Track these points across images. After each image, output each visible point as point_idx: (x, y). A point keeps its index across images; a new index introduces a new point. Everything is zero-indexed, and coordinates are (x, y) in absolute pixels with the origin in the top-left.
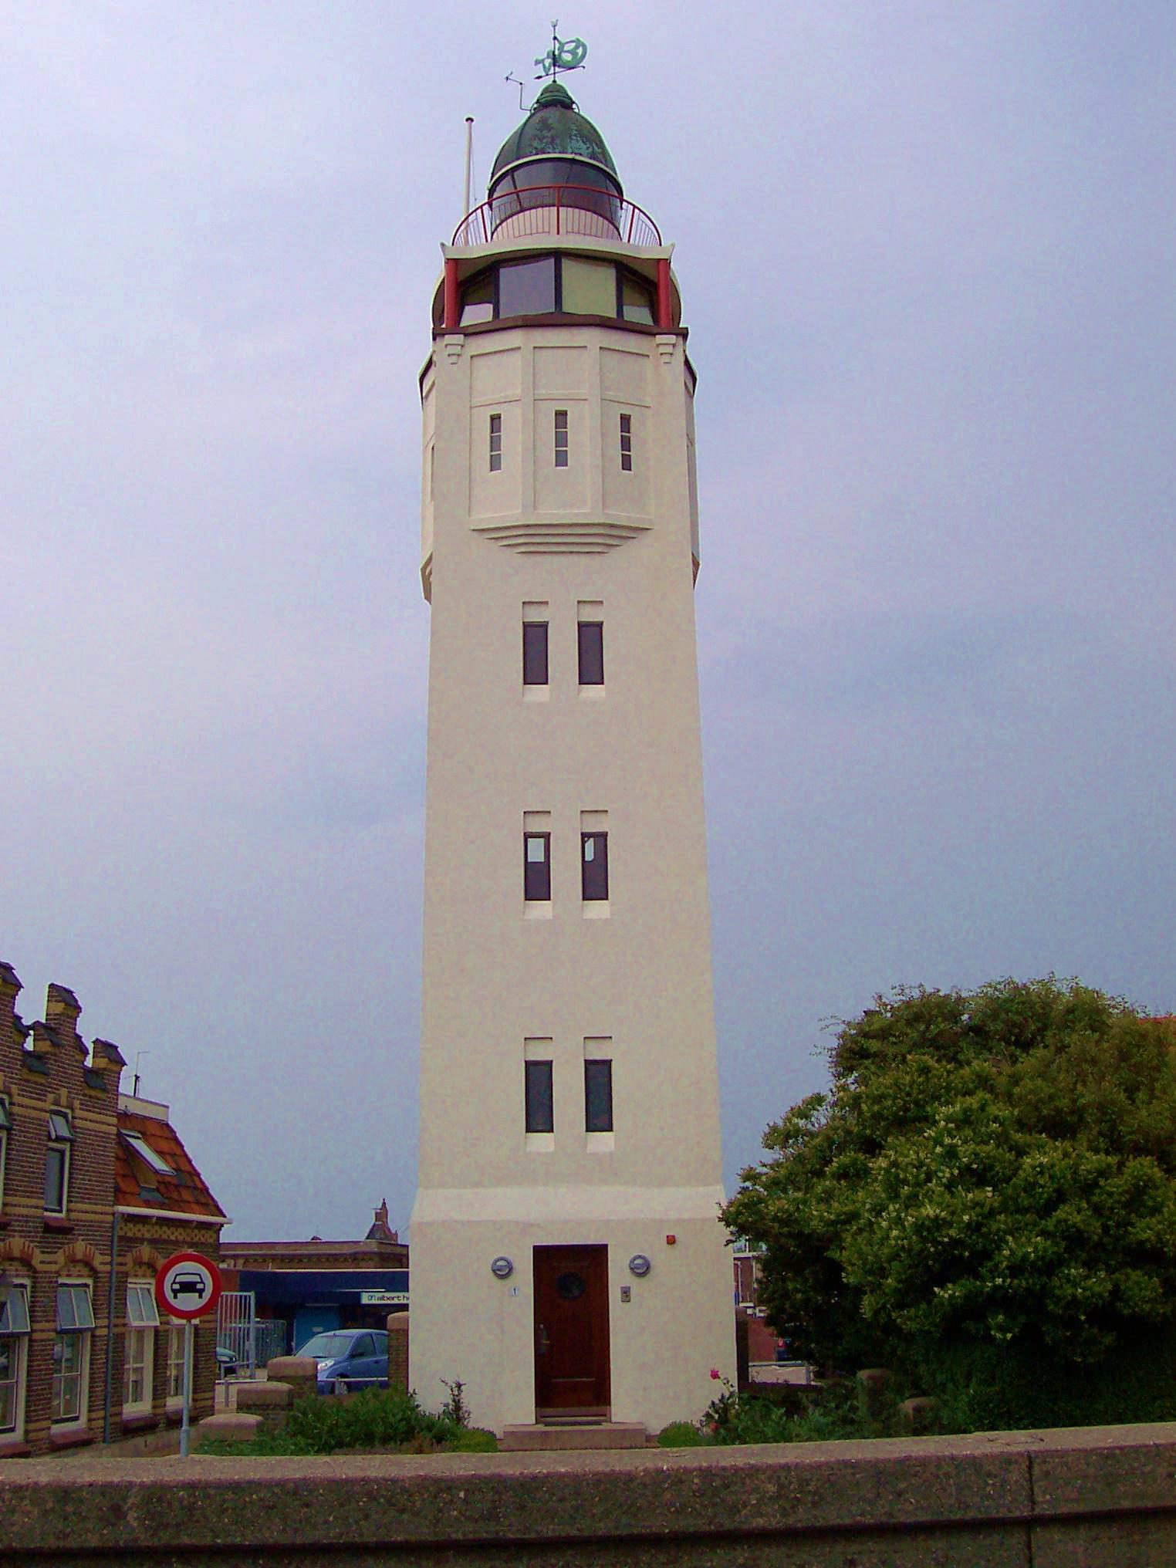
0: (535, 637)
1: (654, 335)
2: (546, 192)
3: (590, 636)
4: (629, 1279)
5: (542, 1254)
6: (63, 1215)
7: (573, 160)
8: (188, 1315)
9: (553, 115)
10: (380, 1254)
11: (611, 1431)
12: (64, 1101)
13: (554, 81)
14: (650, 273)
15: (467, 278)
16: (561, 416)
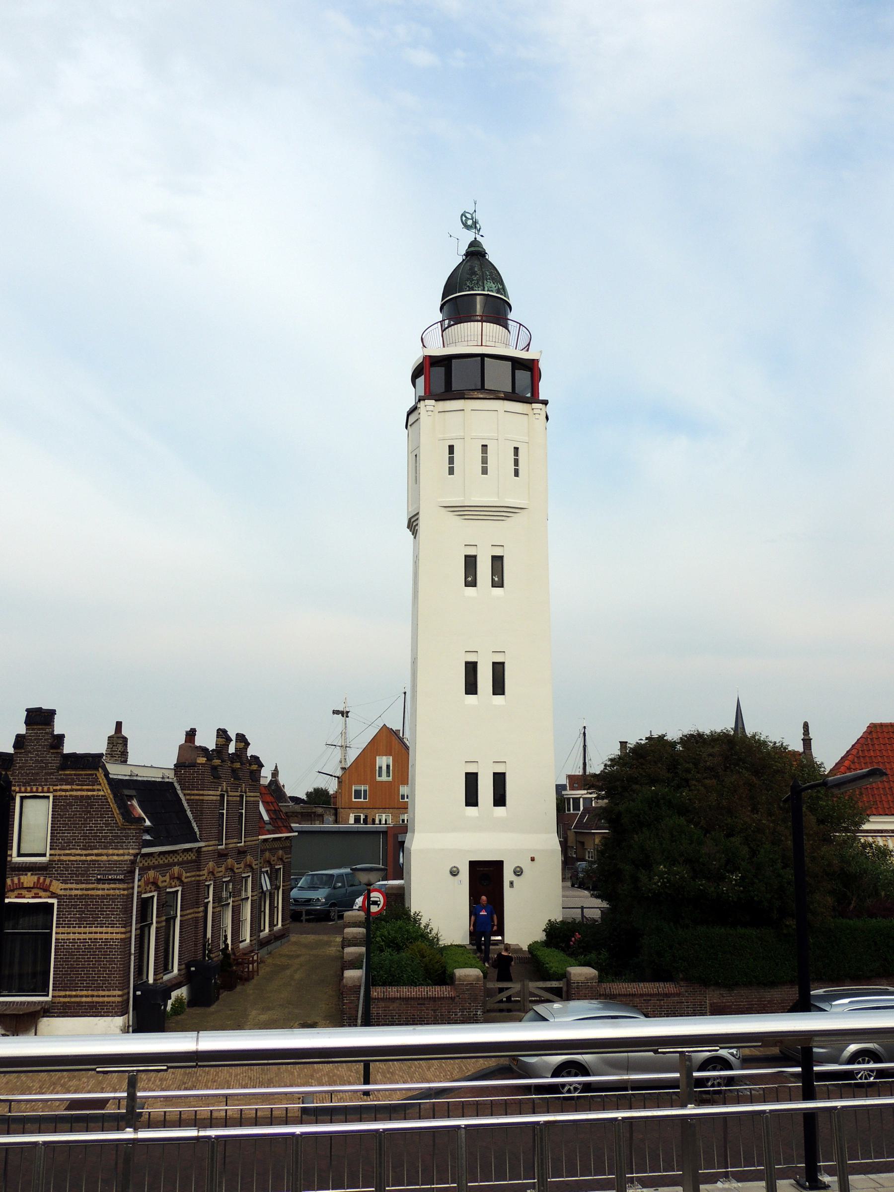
0: (471, 562)
1: (531, 403)
2: (860, 1187)
3: (497, 561)
4: (513, 877)
5: (473, 865)
6: (223, 847)
7: (488, 294)
9: (476, 264)
12: (224, 789)
13: (475, 238)
15: (445, 379)
16: (485, 447)
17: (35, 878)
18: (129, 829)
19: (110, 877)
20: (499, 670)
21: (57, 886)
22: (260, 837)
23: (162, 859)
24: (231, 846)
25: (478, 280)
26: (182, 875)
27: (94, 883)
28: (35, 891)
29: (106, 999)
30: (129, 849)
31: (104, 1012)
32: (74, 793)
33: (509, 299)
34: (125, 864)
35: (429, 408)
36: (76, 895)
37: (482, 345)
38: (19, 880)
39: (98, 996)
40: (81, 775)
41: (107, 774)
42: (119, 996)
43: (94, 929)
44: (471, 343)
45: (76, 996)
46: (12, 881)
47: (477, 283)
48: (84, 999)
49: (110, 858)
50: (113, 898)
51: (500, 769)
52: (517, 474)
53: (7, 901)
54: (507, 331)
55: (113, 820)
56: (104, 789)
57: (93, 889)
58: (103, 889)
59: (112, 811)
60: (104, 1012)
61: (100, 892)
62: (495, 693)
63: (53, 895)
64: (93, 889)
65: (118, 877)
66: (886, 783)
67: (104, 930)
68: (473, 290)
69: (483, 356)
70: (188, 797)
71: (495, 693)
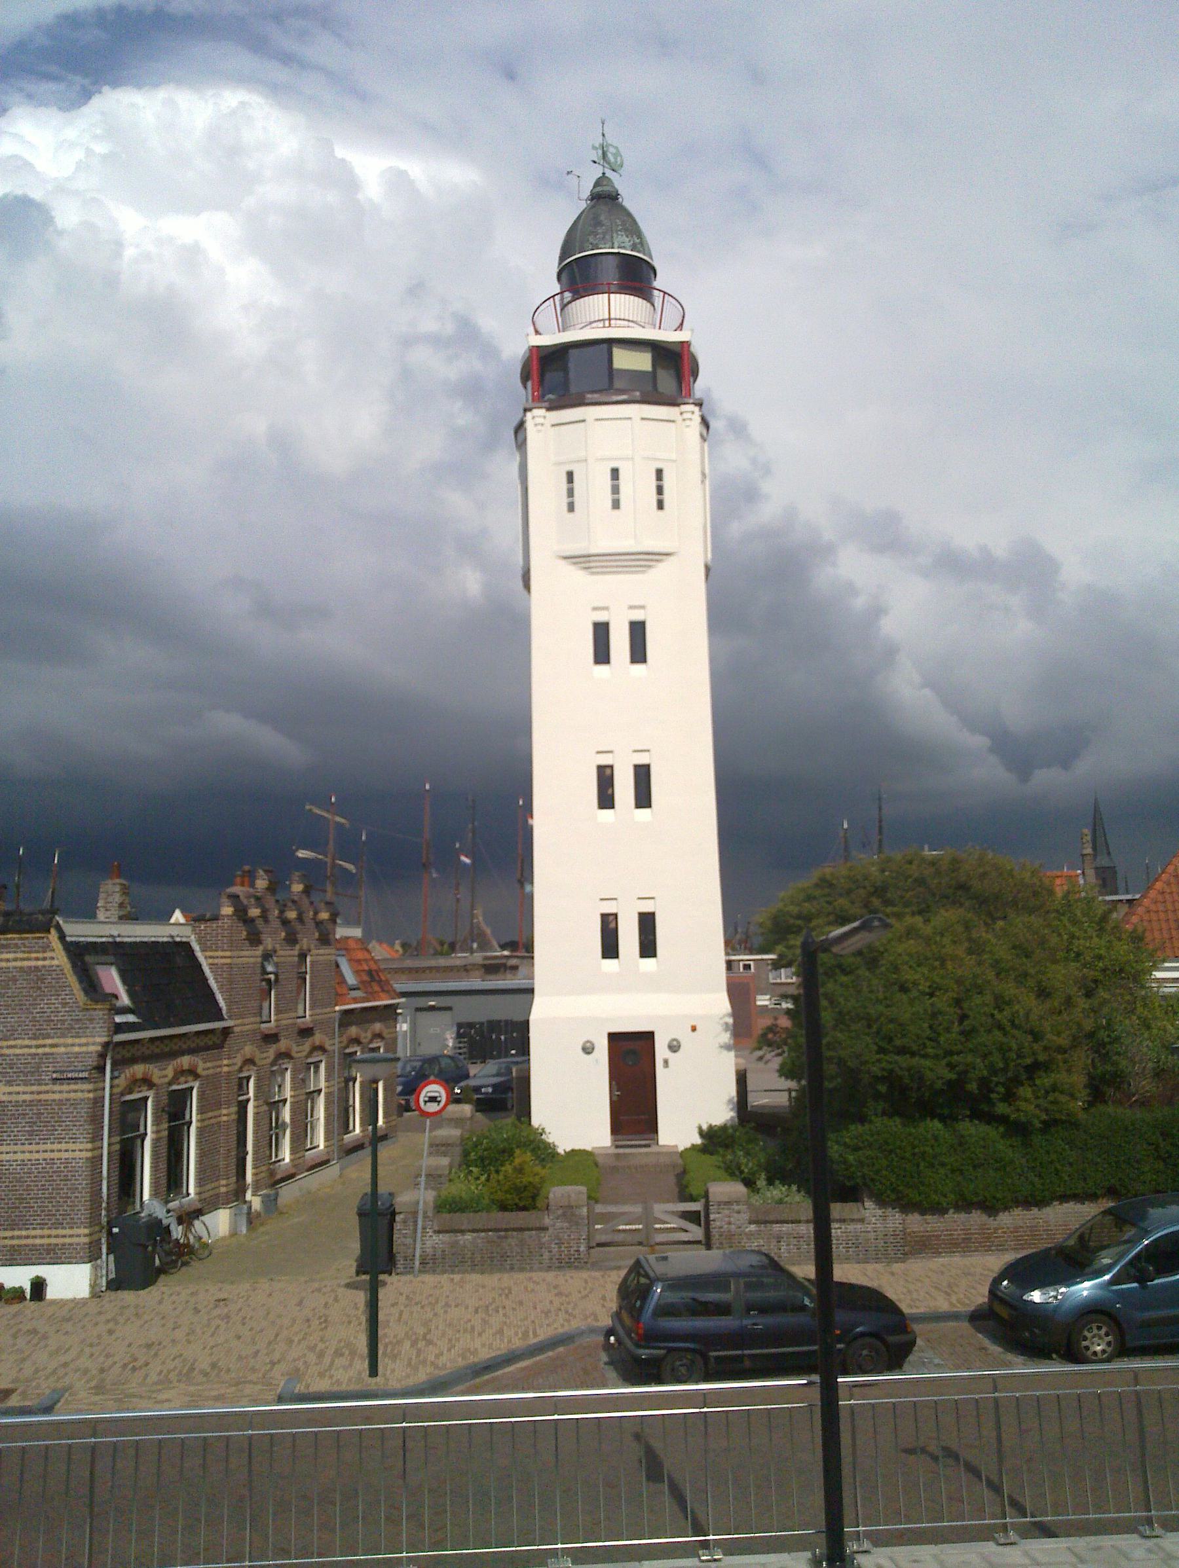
0: (601, 632)
5: (614, 1038)
7: (619, 253)
10: (484, 966)
11: (658, 1153)
13: (604, 174)
14: (678, 349)
20: (643, 774)
22: (337, 1008)
23: (157, 1047)
24: (284, 1022)
25: (604, 234)
26: (196, 1066)
27: (47, 1084)
29: (67, 1240)
30: (94, 1036)
31: (65, 1258)
32: (19, 964)
33: (652, 259)
35: (539, 420)
36: (24, 1101)
39: (57, 1236)
40: (27, 938)
41: (62, 937)
42: (85, 1236)
43: (49, 1146)
45: (27, 1237)
47: (604, 238)
48: (38, 1241)
49: (69, 1049)
50: (75, 1104)
51: (647, 907)
52: (660, 505)
54: (649, 305)
57: (47, 1092)
59: (71, 986)
60: (65, 1258)
61: (57, 1096)
62: (639, 805)
64: (47, 1092)
66: (1152, 914)
67: (63, 1146)
69: (611, 342)
70: (211, 961)
71: (639, 805)
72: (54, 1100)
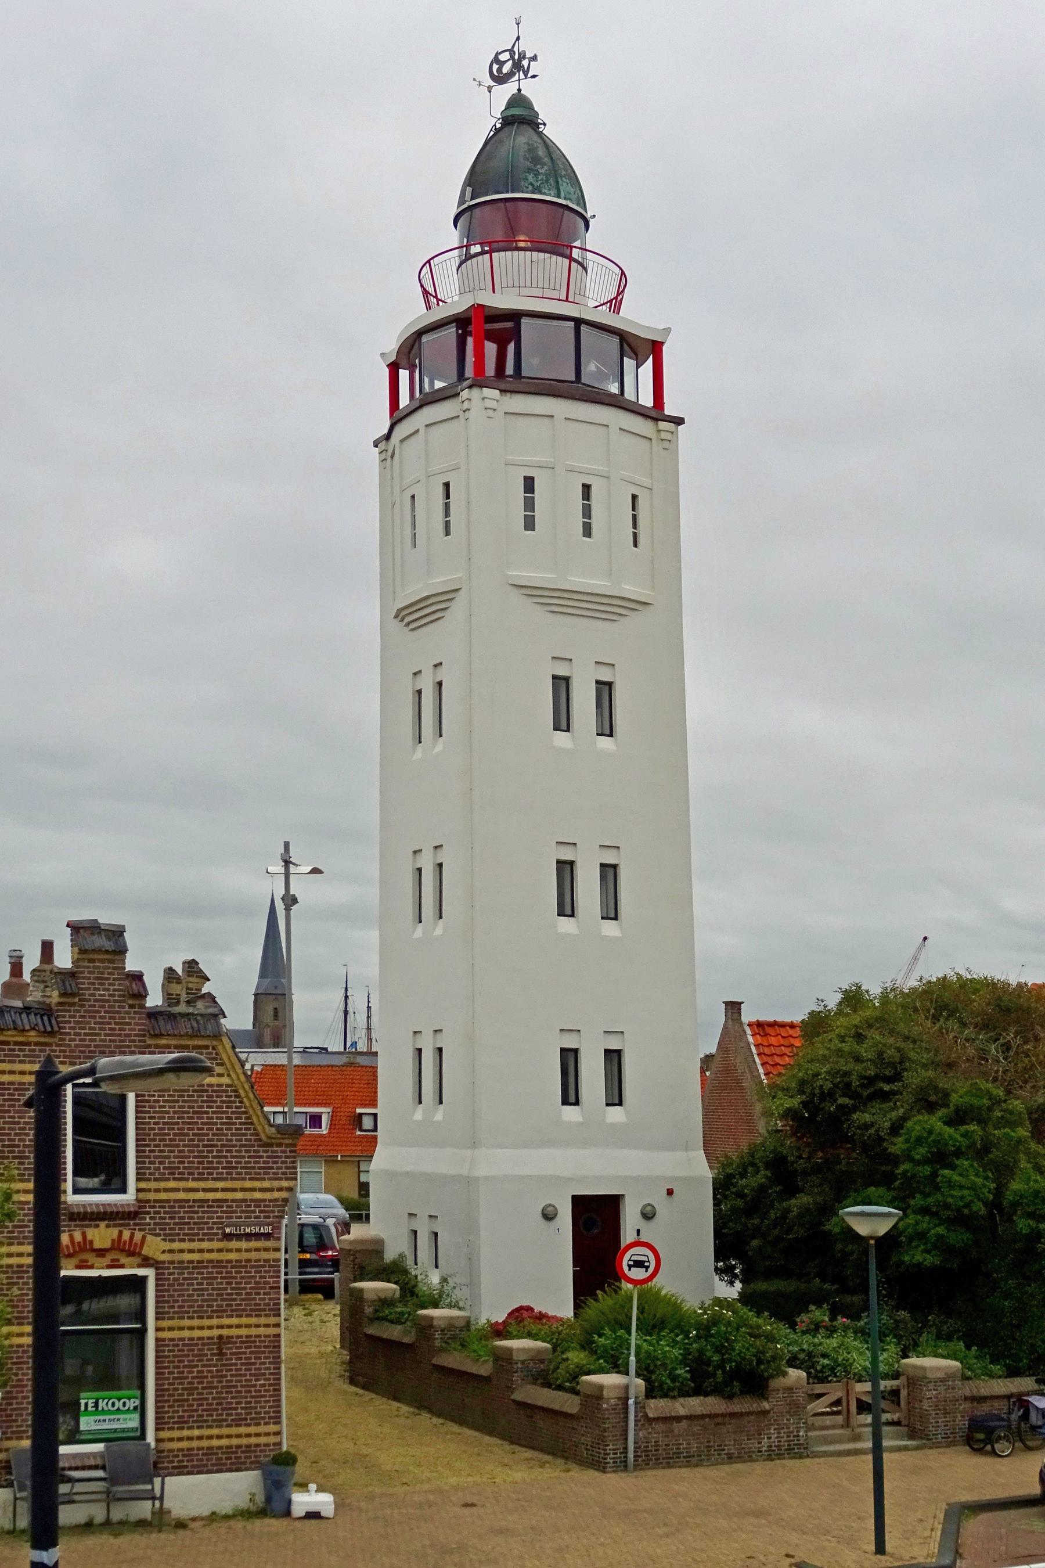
8: (635, 1282)
13: (519, 90)
17: (114, 1232)
18: (280, 1145)
19: (248, 1230)
21: (155, 1246)
28: (113, 1255)
29: (253, 1440)
34: (274, 1206)
35: (489, 404)
37: (567, 300)
38: (84, 1235)
44: (525, 291)
46: (71, 1237)
53: (63, 1273)
55: (249, 1129)
56: (231, 1073)
58: (239, 1250)
63: (146, 1262)
65: (262, 1231)
68: (541, 193)
72: (229, 1261)
